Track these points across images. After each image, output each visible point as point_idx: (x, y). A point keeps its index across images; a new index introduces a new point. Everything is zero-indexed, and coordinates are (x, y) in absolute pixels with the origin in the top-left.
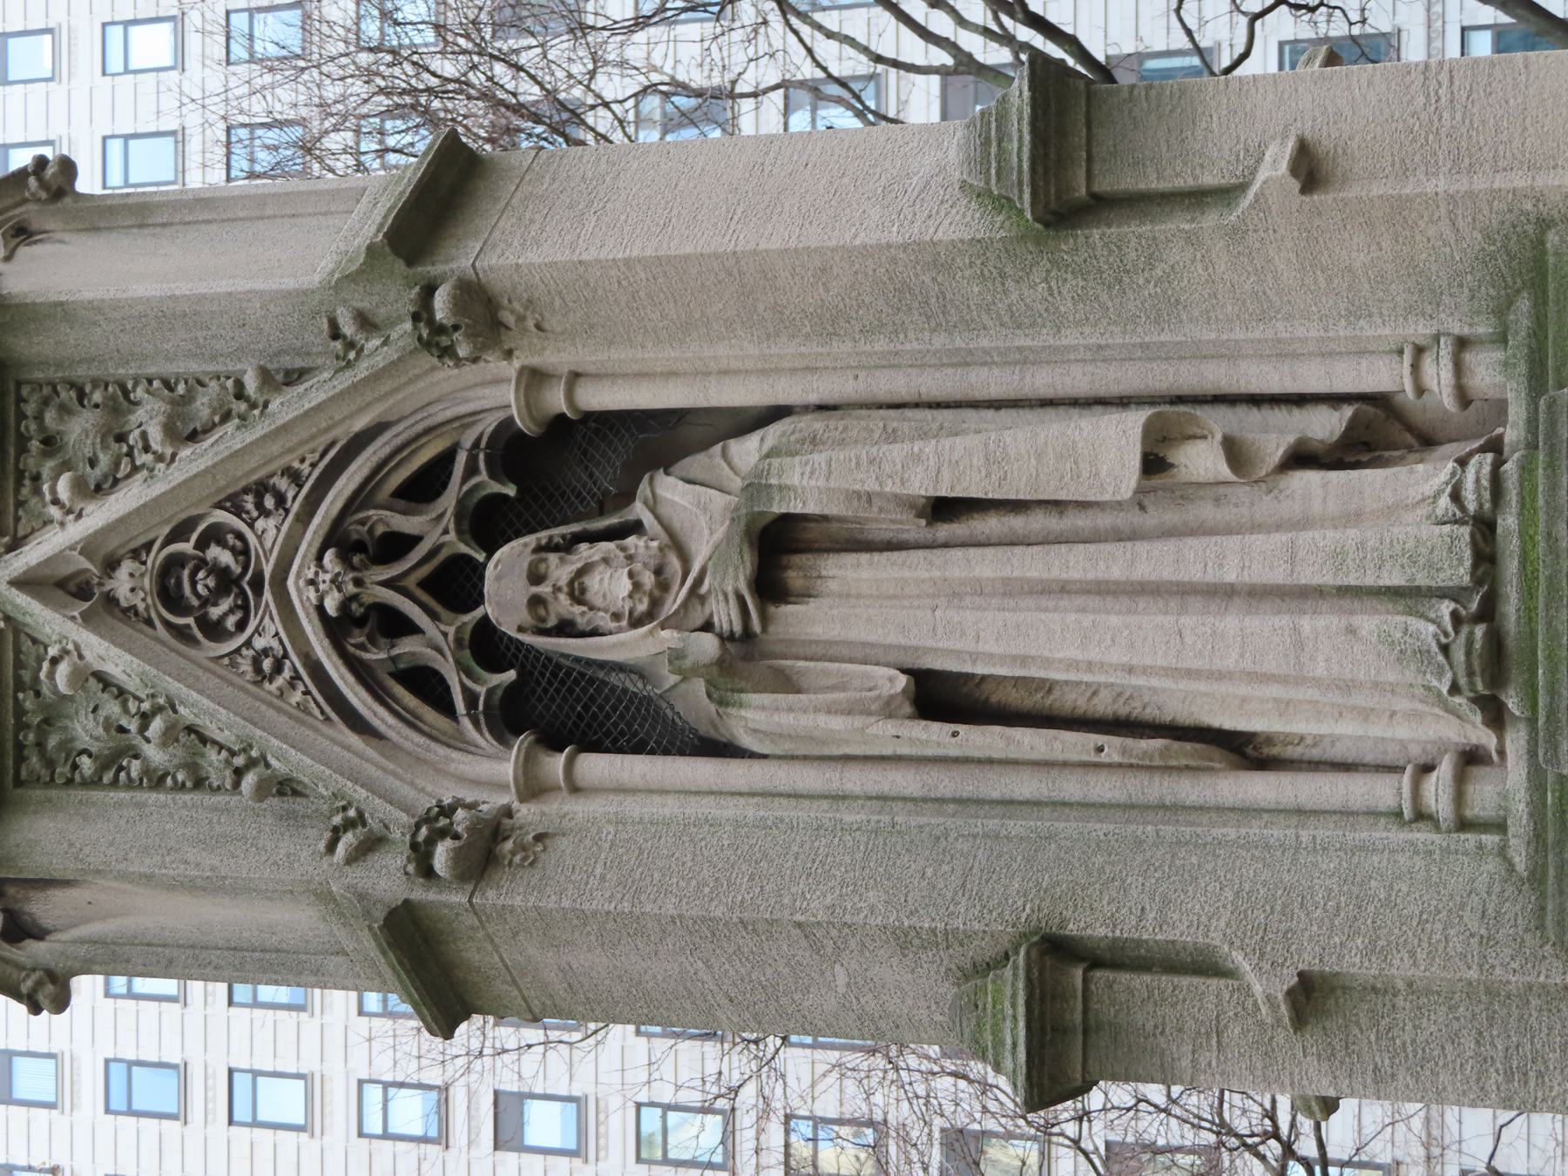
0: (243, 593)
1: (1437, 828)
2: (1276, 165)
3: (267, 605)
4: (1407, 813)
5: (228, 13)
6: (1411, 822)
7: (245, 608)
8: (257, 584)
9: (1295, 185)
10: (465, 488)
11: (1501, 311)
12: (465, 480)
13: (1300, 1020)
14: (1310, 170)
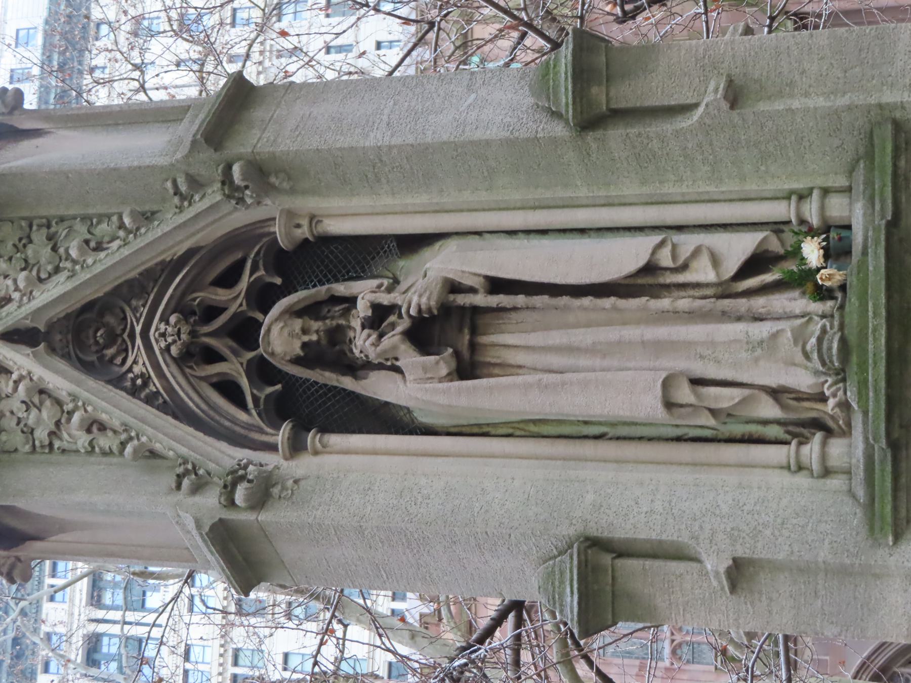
0: (124, 341)
1: (812, 476)
2: (713, 93)
3: (139, 348)
4: (793, 468)
5: (18, 31)
6: (795, 472)
7: (126, 350)
8: (132, 336)
9: (725, 105)
10: (252, 279)
11: (851, 172)
12: (251, 275)
13: (733, 588)
14: (735, 96)
